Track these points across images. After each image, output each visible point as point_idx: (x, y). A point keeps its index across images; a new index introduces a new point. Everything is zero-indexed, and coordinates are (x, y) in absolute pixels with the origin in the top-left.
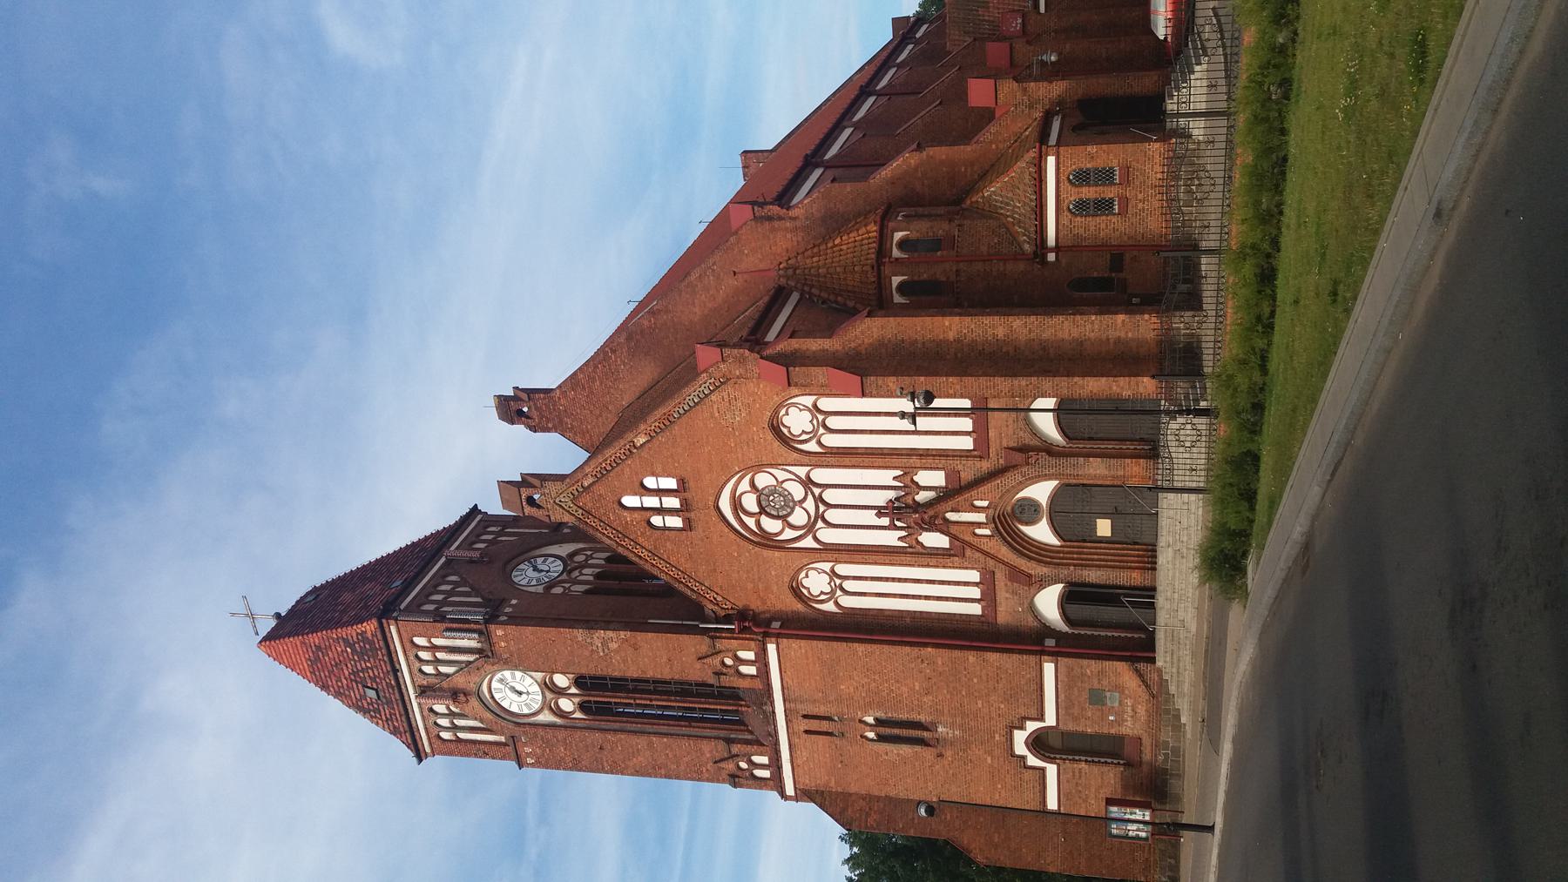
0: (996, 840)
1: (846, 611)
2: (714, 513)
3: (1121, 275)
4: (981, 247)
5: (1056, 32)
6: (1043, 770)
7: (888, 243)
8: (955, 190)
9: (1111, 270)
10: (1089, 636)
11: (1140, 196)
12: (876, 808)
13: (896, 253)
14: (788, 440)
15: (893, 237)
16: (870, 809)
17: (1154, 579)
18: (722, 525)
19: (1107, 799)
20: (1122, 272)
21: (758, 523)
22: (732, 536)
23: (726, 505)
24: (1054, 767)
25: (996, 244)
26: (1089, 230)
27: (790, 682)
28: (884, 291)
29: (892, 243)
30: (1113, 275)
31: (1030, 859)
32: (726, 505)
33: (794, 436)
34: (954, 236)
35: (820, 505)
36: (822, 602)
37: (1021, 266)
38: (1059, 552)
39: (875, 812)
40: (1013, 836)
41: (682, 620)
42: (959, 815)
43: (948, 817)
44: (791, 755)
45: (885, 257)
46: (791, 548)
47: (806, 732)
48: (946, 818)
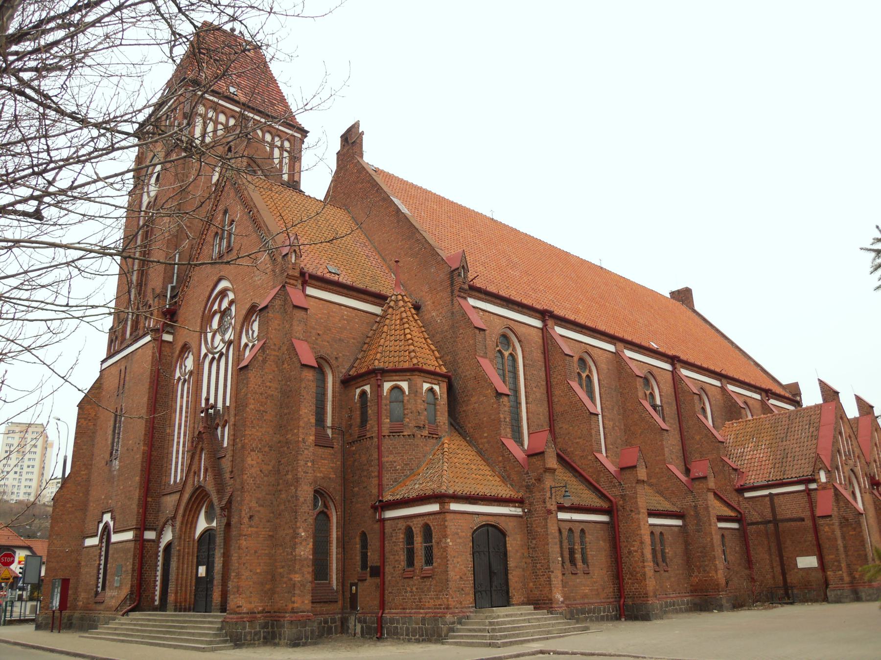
0: (68, 505)
1: (175, 387)
2: (215, 279)
3: (368, 578)
4: (392, 456)
5: (695, 506)
6: (96, 536)
7: (397, 378)
8: (472, 430)
9: (371, 567)
10: (157, 563)
11: (414, 589)
12: (89, 424)
13: (387, 386)
14: (248, 320)
15: (404, 381)
16: (90, 420)
17: (668, 610)
18: (212, 285)
19: (69, 580)
20: (370, 576)
21: (215, 312)
22: (207, 294)
23: (223, 284)
24: (97, 543)
25: (396, 467)
26: (394, 546)
27: (137, 354)
28: (361, 379)
29: (398, 381)
30: (369, 569)
31: (56, 528)
32: (223, 284)
33: (252, 325)
34: (402, 432)
35: (218, 354)
36: (181, 368)
37: (375, 491)
38: (190, 537)
39: (87, 423)
40: (70, 516)
41: (177, 273)
42: (84, 480)
43: (83, 473)
44: (754, 398)
45: (381, 376)
46: (201, 339)
47: (121, 370)
48: (82, 471)
